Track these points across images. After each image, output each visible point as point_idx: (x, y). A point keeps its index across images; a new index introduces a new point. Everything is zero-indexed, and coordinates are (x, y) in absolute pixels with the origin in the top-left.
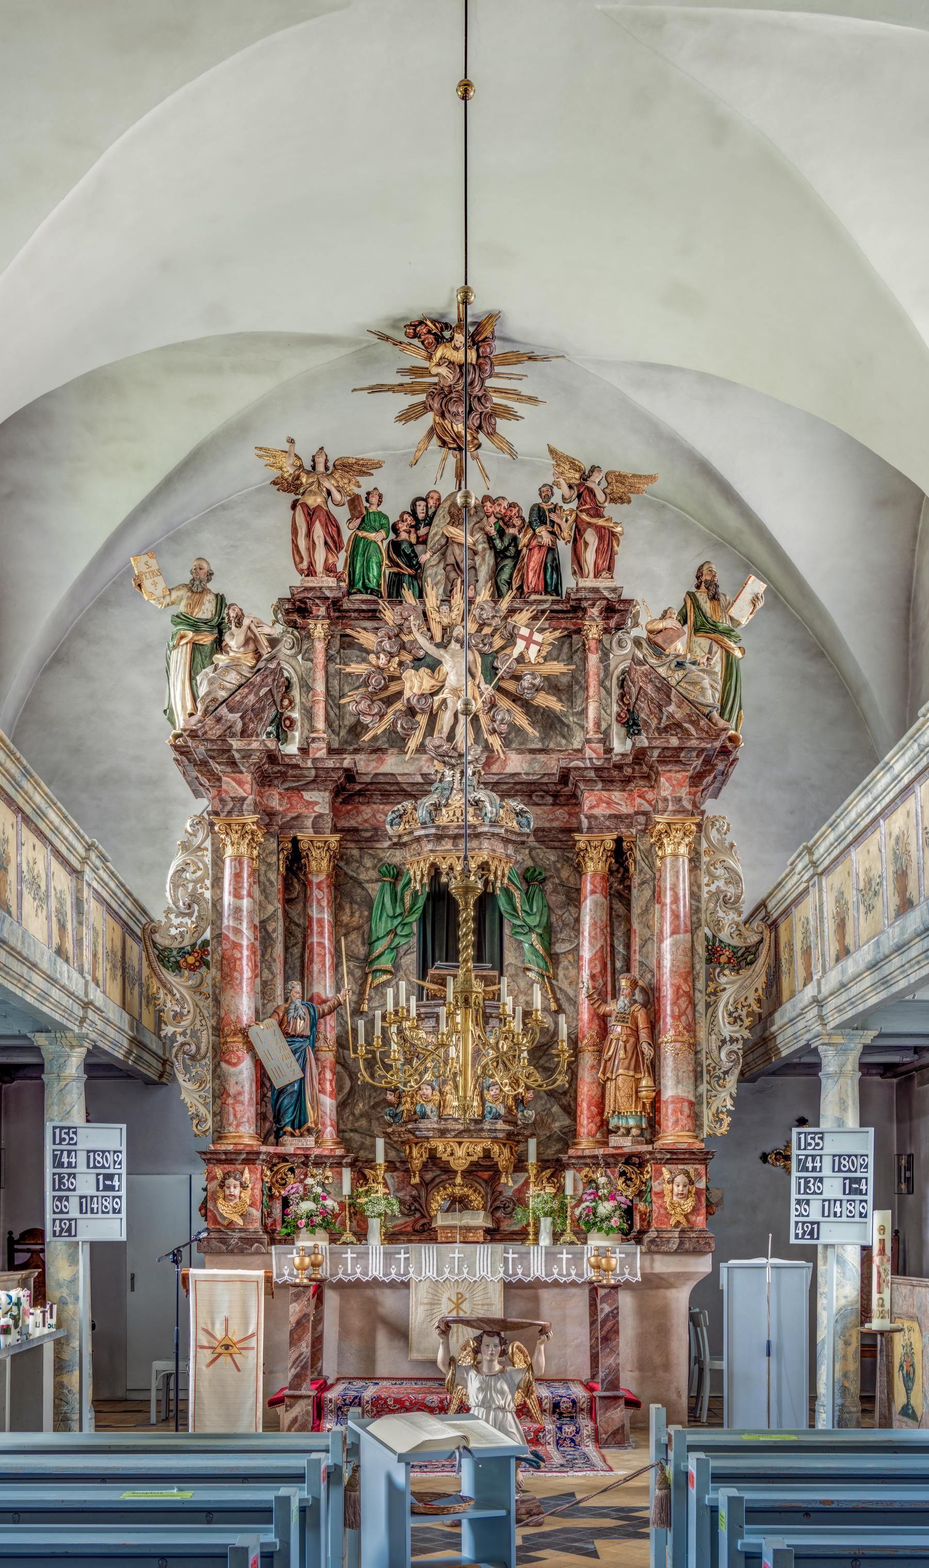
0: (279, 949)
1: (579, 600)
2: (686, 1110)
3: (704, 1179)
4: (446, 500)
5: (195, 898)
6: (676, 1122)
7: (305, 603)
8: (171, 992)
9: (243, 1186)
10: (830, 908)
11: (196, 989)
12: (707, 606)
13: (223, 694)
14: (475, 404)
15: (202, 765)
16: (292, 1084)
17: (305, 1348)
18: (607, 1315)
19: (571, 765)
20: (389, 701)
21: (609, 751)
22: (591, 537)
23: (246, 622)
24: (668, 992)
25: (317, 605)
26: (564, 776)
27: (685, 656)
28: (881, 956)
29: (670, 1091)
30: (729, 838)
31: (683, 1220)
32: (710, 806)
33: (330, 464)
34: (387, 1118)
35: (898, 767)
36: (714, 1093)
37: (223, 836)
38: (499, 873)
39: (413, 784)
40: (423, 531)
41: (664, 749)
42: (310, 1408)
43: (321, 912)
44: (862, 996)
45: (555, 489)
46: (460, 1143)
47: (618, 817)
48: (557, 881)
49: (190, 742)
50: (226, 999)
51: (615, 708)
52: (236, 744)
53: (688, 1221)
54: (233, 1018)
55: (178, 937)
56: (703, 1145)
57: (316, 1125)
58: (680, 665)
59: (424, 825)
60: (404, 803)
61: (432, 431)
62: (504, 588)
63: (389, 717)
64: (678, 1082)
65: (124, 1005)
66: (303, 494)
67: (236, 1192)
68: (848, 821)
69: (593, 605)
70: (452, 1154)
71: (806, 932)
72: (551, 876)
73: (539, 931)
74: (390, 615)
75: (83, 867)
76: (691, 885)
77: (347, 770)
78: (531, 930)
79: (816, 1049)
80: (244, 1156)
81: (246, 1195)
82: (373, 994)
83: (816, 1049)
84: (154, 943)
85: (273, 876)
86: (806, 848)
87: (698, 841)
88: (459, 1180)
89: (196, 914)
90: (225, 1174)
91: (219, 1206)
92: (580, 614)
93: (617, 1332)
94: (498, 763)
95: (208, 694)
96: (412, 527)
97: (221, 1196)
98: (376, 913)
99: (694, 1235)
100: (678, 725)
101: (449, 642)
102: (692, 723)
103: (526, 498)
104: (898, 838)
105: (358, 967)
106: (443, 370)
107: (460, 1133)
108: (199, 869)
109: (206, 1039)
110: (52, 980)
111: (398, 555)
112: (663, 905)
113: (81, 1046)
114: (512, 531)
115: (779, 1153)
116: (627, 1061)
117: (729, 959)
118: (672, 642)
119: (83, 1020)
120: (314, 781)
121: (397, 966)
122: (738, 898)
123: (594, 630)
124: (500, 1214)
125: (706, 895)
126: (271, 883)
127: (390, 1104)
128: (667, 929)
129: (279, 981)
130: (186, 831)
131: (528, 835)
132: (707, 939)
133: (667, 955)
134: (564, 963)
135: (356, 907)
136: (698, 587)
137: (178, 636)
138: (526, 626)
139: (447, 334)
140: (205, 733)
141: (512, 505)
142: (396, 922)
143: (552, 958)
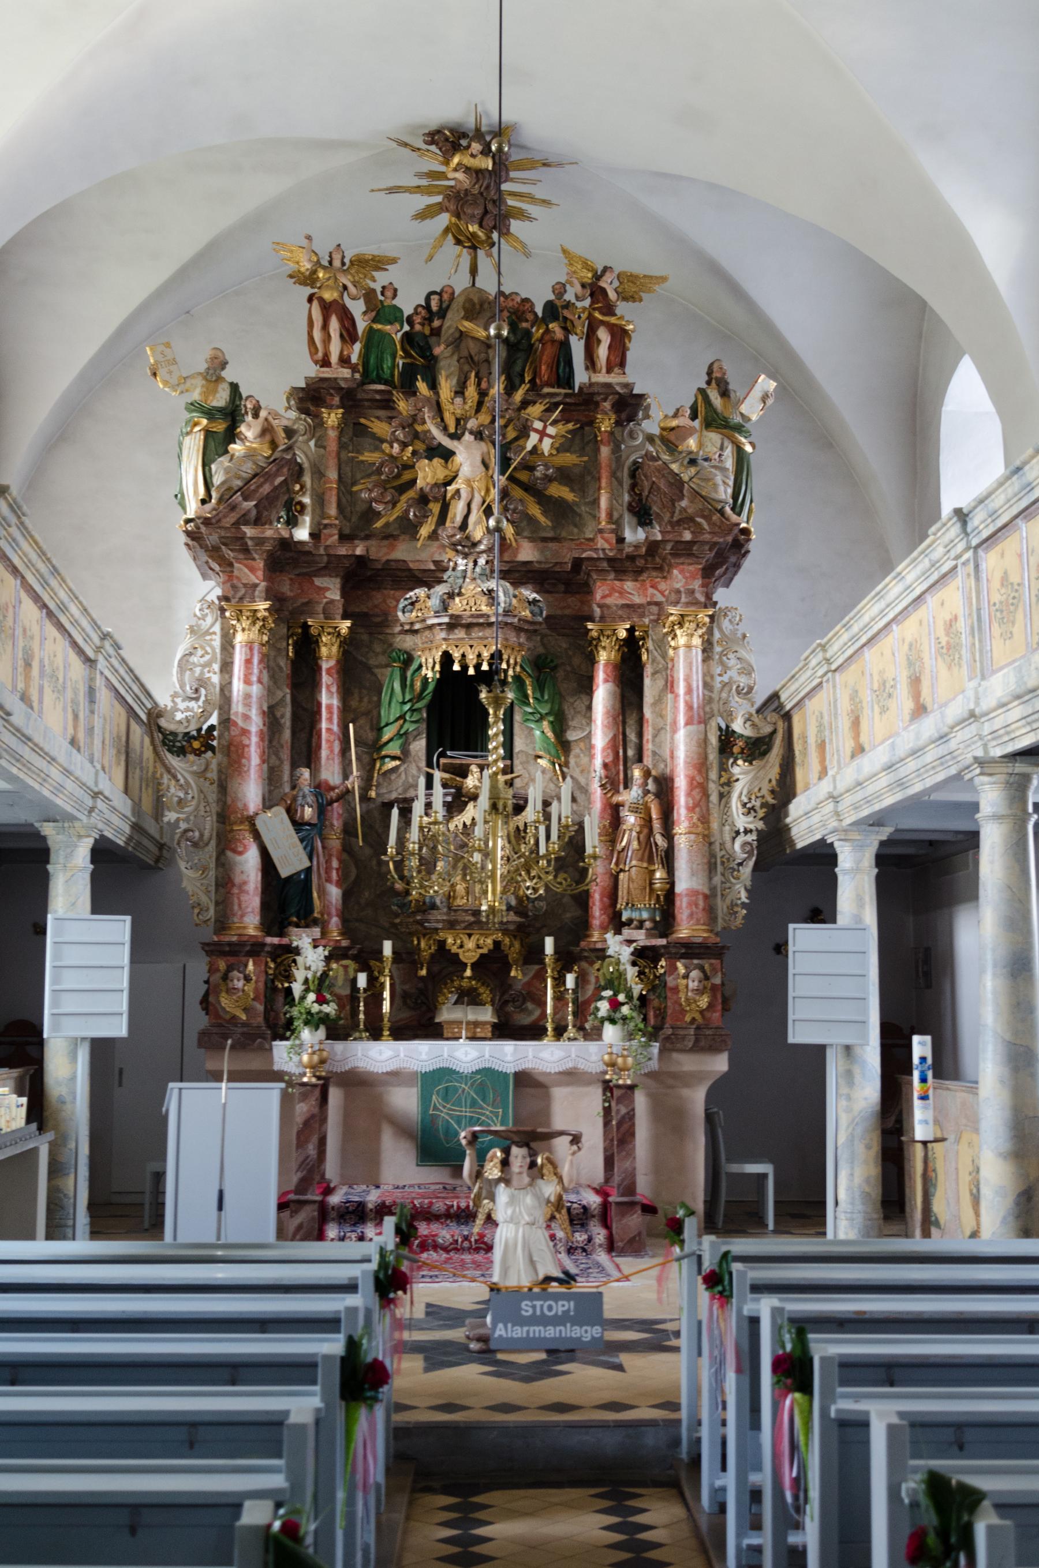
0: (287, 734)
1: (593, 394)
2: (701, 903)
3: (719, 974)
4: (459, 295)
5: (202, 683)
6: (691, 915)
7: (320, 392)
8: (175, 777)
9: (247, 979)
10: (844, 705)
11: (202, 774)
12: (714, 396)
13: (239, 483)
14: (490, 207)
15: (214, 552)
16: (298, 873)
17: (311, 1149)
18: (623, 1117)
19: (584, 556)
21: (621, 540)
22: (603, 335)
23: (263, 414)
24: (681, 784)
25: (332, 395)
26: (578, 563)
27: (698, 452)
28: (896, 758)
29: (682, 886)
30: (741, 629)
31: (698, 1016)
32: (721, 595)
33: (347, 261)
34: (394, 908)
35: (910, 578)
36: (728, 885)
37: (234, 622)
38: (512, 661)
40: (436, 323)
41: (677, 542)
42: (316, 1213)
43: (328, 698)
44: (878, 796)
45: (568, 287)
46: (470, 936)
47: (630, 607)
48: (568, 668)
49: (203, 529)
50: (232, 786)
51: (626, 497)
52: (249, 531)
54: (240, 805)
55: (184, 722)
56: (718, 940)
57: (322, 915)
58: (693, 462)
60: (417, 591)
61: (447, 230)
62: (517, 381)
63: (402, 505)
64: (693, 874)
65: (126, 791)
66: (319, 288)
67: (239, 984)
69: (605, 400)
70: (461, 946)
71: (820, 725)
72: (563, 664)
74: (403, 406)
75: (96, 655)
76: (704, 675)
77: (359, 558)
78: (542, 718)
79: (832, 844)
80: (248, 948)
81: (249, 988)
82: (381, 780)
83: (832, 844)
85: (282, 662)
86: (820, 645)
87: (710, 632)
88: (468, 973)
89: (203, 698)
91: (222, 1000)
92: (592, 407)
93: (633, 1134)
94: (510, 551)
95: (223, 483)
96: (425, 319)
97: (224, 988)
98: (385, 697)
99: (708, 1032)
100: (691, 519)
101: (463, 434)
102: (704, 517)
103: (540, 297)
104: (911, 645)
105: (367, 753)
106: (460, 175)
108: (207, 653)
109: (209, 825)
110: (67, 772)
111: (412, 347)
112: (677, 696)
113: (89, 836)
114: (524, 325)
116: (641, 852)
117: (743, 749)
118: (685, 439)
119: (91, 810)
120: (325, 568)
122: (751, 689)
125: (719, 686)
126: (280, 668)
127: (397, 894)
128: (682, 719)
129: (286, 768)
130: (195, 615)
131: (540, 623)
132: (720, 729)
133: (678, 746)
134: (575, 751)
135: (365, 692)
136: (709, 383)
137: (191, 424)
138: (540, 420)
139: (464, 142)
140: (219, 521)
141: (526, 300)
142: (407, 707)
143: (563, 746)
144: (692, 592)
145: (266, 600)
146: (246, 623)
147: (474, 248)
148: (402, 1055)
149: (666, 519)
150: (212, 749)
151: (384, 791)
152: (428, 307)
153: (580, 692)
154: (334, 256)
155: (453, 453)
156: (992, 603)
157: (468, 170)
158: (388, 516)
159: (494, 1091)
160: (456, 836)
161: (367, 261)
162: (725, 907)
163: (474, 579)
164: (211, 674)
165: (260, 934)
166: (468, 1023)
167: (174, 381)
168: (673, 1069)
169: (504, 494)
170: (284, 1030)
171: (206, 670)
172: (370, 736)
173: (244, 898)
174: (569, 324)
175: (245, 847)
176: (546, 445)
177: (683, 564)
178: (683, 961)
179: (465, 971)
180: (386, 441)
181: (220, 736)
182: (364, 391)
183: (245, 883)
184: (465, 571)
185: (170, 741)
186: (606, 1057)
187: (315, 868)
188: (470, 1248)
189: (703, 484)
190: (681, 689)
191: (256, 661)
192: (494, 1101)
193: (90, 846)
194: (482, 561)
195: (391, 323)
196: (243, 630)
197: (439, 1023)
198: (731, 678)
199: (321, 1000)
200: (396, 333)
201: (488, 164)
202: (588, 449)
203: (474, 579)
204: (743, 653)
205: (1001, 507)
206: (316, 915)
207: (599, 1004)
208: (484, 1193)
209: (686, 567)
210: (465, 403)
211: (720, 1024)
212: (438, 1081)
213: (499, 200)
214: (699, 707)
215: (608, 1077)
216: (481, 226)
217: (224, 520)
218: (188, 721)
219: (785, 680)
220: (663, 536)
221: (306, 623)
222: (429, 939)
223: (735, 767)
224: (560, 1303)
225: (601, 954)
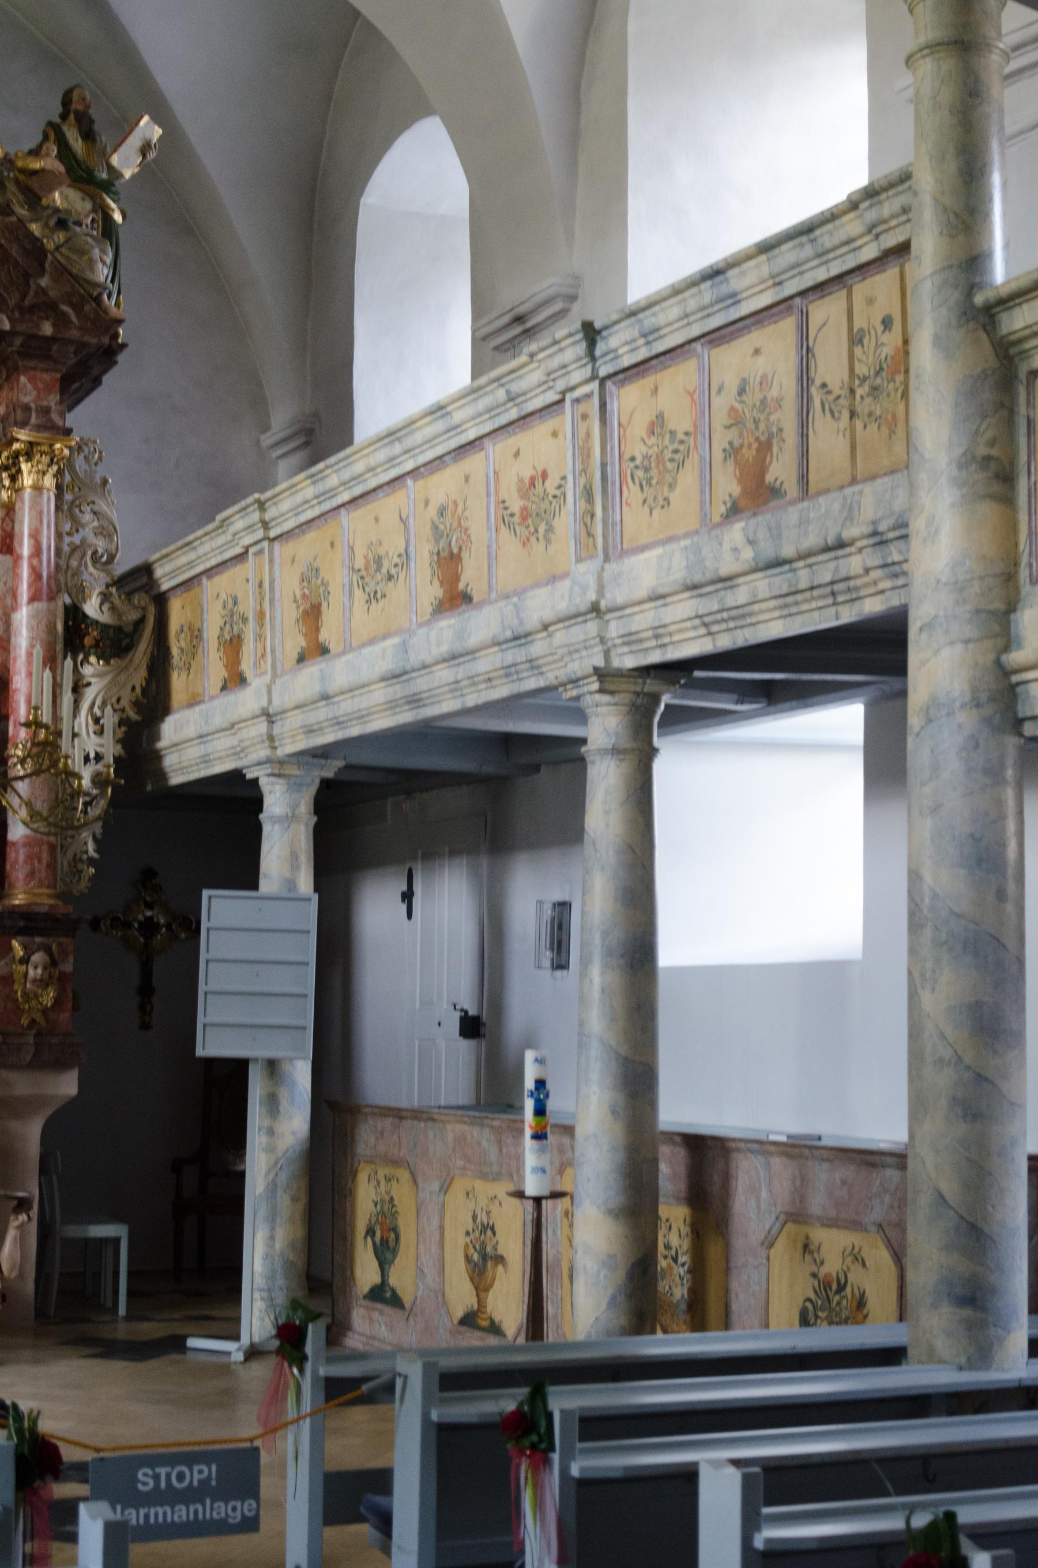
3: (71, 959)
6: (31, 875)
10: (288, 585)
12: (77, 144)
31: (39, 1017)
32: (80, 419)
53: (47, 1020)
58: (62, 224)
68: (346, 475)
79: (255, 781)
83: (255, 781)
104: (442, 512)
117: (97, 642)
118: (51, 190)
136: (64, 117)
144: (46, 411)
149: (12, 302)
156: (627, 456)
162: (65, 864)
177: (34, 369)
178: (20, 938)
189: (74, 257)
190: (25, 549)
198: (83, 541)
204: (102, 506)
205: (670, 324)
209: (38, 374)
214: (49, 577)
220: (11, 326)
223: (86, 665)
224: (196, 1468)
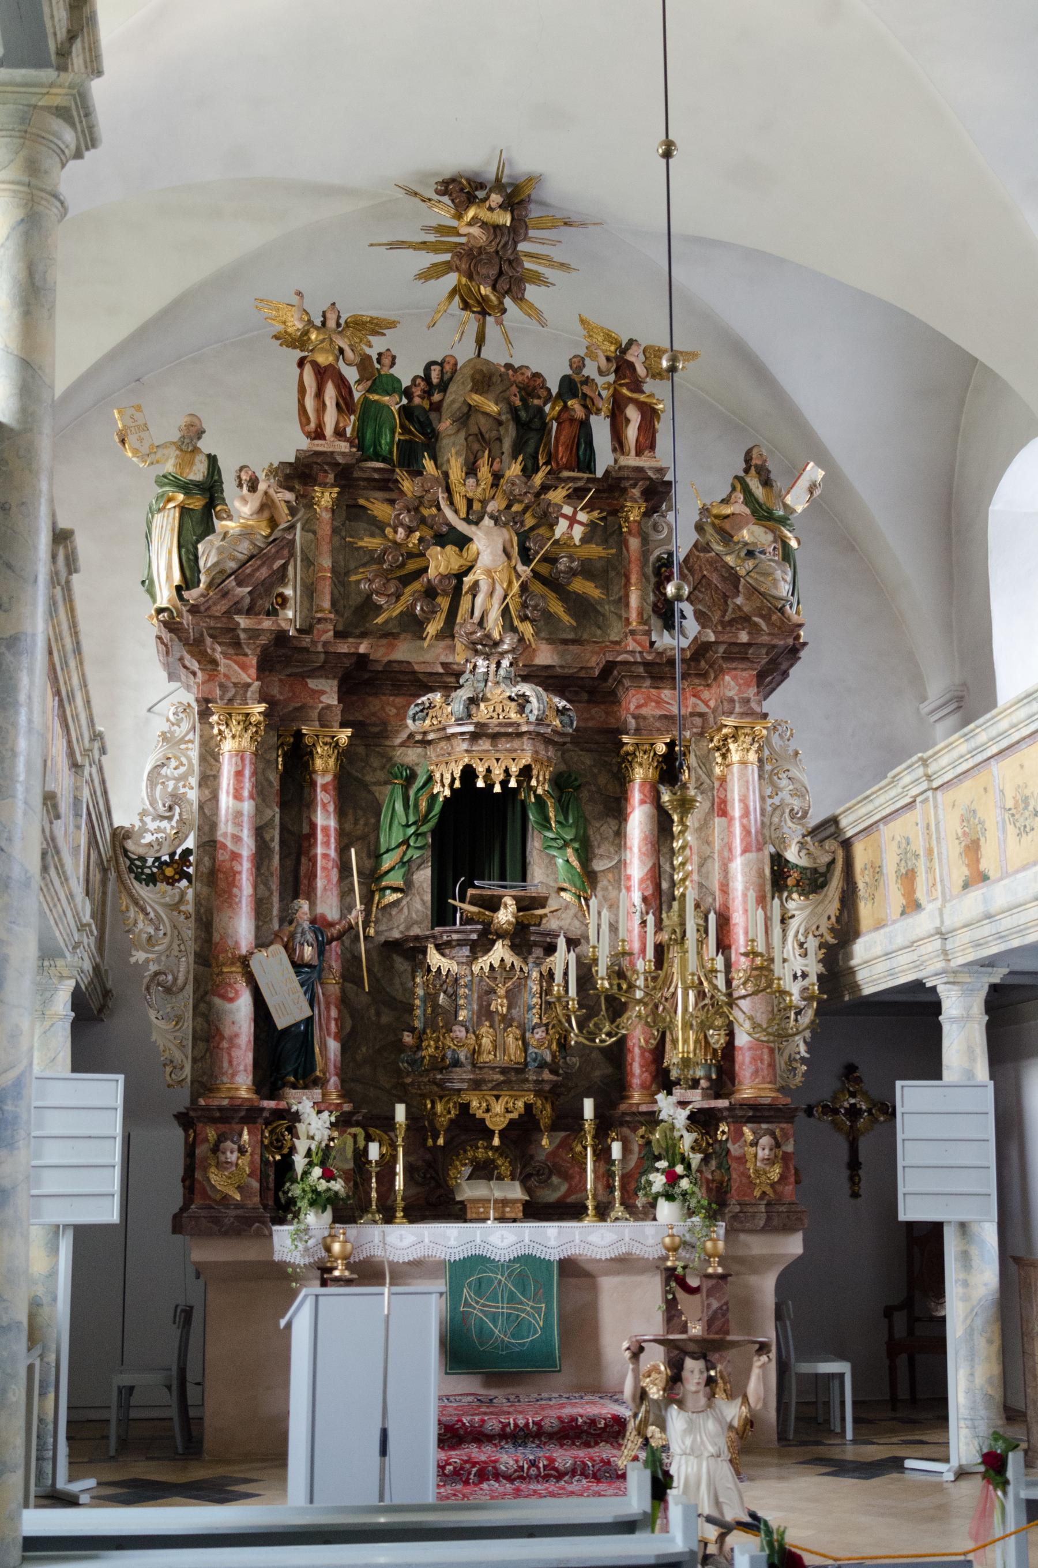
1: (620, 479)
3: (792, 1141)
4: (464, 366)
5: (176, 800)
6: (756, 1072)
8: (143, 910)
9: (242, 1151)
10: (951, 825)
12: (758, 490)
13: (232, 565)
14: (505, 267)
15: (196, 647)
16: (297, 1025)
18: (715, 1312)
20: (407, 580)
22: (633, 414)
25: (326, 471)
26: (609, 667)
30: (793, 745)
31: (768, 1190)
33: (342, 321)
39: (431, 674)
40: (437, 397)
43: (325, 819)
45: (587, 361)
46: (497, 1097)
47: (669, 718)
52: (243, 622)
53: (775, 1191)
54: (231, 943)
55: (155, 844)
56: (788, 1100)
58: (750, 554)
59: (460, 721)
61: (454, 291)
67: (233, 1157)
69: (634, 486)
70: (488, 1110)
73: (576, 845)
78: (566, 844)
80: (243, 1114)
81: (244, 1162)
84: (126, 852)
86: (921, 759)
89: (177, 817)
90: (219, 1136)
95: (215, 565)
96: (425, 392)
98: (385, 820)
106: (475, 231)
107: (498, 1086)
108: (182, 764)
109: (185, 968)
114: (536, 402)
115: (825, 1107)
117: (798, 881)
118: (741, 528)
120: (321, 667)
121: (409, 883)
122: (805, 814)
123: (636, 512)
124: (533, 1182)
126: (270, 783)
129: (276, 899)
130: (168, 720)
134: (603, 883)
135: (360, 813)
136: (747, 471)
137: (165, 498)
140: (208, 608)
141: (537, 375)
142: (412, 830)
143: (589, 878)
144: (747, 701)
145: (259, 702)
146: (236, 729)
147: (484, 313)
148: (427, 1240)
150: (188, 877)
151: (383, 928)
152: (427, 378)
153: (608, 816)
154: (328, 315)
155: (469, 540)
157: (484, 225)
158: (391, 611)
159: (536, 1282)
160: (481, 979)
161: (364, 323)
163: (498, 683)
164: (186, 789)
165: (254, 1096)
166: (496, 1201)
167: (145, 450)
168: (741, 1252)
169: (524, 588)
170: (283, 1210)
171: (181, 784)
172: (368, 864)
173: (235, 1053)
174: (588, 402)
175: (237, 992)
176: (578, 532)
179: (492, 1139)
180: (389, 525)
181: (198, 862)
182: (361, 469)
183: (237, 1035)
184: (487, 673)
185: (137, 867)
186: (667, 1240)
187: (316, 1018)
188: (537, 1476)
190: (736, 811)
191: (247, 773)
192: (535, 1294)
193: (72, 989)
194: (505, 663)
195: (389, 394)
196: (234, 737)
197: (462, 1202)
199: (328, 1176)
200: (394, 403)
201: (506, 219)
202: (611, 541)
203: (498, 683)
204: (795, 772)
206: (318, 1073)
207: (652, 1177)
208: (651, 1419)
210: (478, 484)
211: (794, 1199)
212: (467, 1271)
213: (514, 262)
214: (757, 832)
215: (669, 1264)
216: (494, 288)
217: (214, 608)
218: (160, 844)
219: (854, 801)
221: (299, 731)
222: (448, 1102)
225: (652, 1119)
